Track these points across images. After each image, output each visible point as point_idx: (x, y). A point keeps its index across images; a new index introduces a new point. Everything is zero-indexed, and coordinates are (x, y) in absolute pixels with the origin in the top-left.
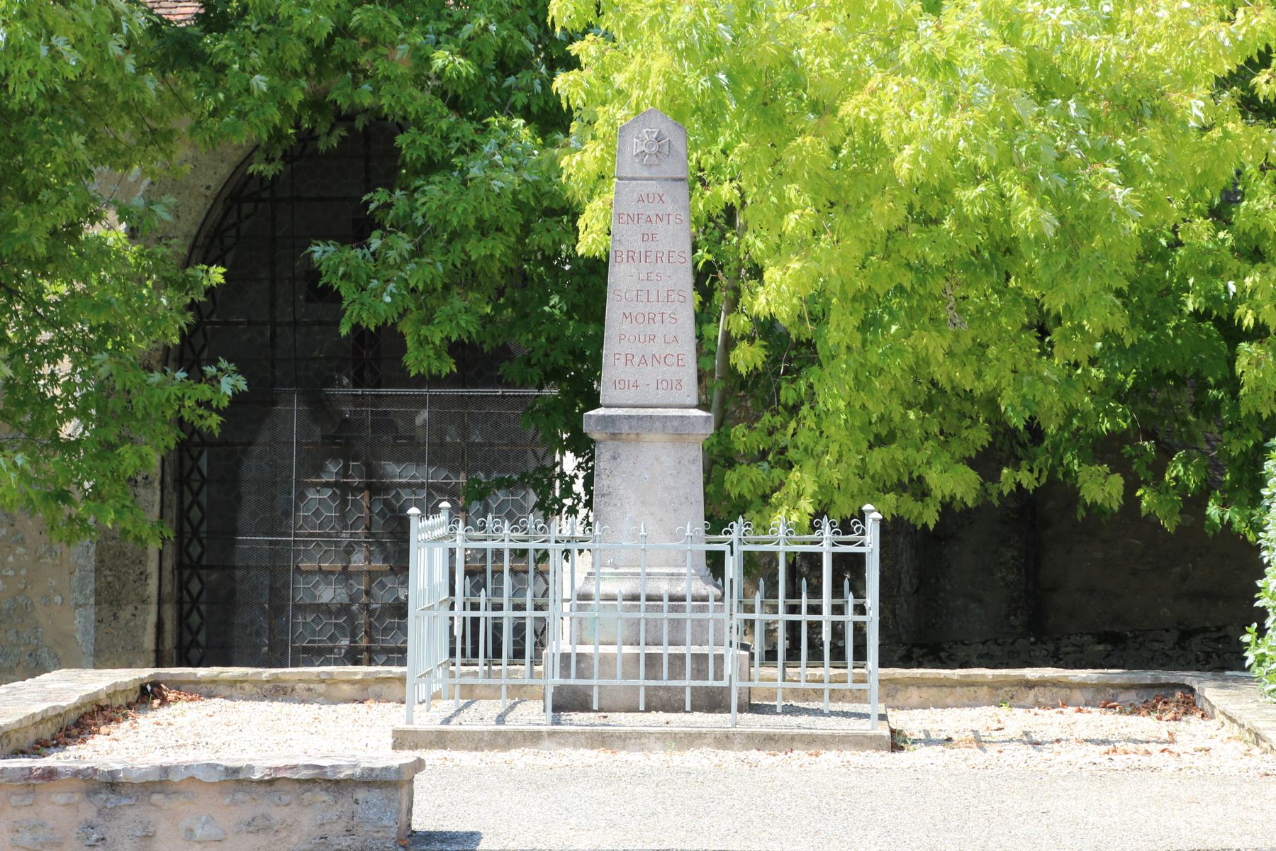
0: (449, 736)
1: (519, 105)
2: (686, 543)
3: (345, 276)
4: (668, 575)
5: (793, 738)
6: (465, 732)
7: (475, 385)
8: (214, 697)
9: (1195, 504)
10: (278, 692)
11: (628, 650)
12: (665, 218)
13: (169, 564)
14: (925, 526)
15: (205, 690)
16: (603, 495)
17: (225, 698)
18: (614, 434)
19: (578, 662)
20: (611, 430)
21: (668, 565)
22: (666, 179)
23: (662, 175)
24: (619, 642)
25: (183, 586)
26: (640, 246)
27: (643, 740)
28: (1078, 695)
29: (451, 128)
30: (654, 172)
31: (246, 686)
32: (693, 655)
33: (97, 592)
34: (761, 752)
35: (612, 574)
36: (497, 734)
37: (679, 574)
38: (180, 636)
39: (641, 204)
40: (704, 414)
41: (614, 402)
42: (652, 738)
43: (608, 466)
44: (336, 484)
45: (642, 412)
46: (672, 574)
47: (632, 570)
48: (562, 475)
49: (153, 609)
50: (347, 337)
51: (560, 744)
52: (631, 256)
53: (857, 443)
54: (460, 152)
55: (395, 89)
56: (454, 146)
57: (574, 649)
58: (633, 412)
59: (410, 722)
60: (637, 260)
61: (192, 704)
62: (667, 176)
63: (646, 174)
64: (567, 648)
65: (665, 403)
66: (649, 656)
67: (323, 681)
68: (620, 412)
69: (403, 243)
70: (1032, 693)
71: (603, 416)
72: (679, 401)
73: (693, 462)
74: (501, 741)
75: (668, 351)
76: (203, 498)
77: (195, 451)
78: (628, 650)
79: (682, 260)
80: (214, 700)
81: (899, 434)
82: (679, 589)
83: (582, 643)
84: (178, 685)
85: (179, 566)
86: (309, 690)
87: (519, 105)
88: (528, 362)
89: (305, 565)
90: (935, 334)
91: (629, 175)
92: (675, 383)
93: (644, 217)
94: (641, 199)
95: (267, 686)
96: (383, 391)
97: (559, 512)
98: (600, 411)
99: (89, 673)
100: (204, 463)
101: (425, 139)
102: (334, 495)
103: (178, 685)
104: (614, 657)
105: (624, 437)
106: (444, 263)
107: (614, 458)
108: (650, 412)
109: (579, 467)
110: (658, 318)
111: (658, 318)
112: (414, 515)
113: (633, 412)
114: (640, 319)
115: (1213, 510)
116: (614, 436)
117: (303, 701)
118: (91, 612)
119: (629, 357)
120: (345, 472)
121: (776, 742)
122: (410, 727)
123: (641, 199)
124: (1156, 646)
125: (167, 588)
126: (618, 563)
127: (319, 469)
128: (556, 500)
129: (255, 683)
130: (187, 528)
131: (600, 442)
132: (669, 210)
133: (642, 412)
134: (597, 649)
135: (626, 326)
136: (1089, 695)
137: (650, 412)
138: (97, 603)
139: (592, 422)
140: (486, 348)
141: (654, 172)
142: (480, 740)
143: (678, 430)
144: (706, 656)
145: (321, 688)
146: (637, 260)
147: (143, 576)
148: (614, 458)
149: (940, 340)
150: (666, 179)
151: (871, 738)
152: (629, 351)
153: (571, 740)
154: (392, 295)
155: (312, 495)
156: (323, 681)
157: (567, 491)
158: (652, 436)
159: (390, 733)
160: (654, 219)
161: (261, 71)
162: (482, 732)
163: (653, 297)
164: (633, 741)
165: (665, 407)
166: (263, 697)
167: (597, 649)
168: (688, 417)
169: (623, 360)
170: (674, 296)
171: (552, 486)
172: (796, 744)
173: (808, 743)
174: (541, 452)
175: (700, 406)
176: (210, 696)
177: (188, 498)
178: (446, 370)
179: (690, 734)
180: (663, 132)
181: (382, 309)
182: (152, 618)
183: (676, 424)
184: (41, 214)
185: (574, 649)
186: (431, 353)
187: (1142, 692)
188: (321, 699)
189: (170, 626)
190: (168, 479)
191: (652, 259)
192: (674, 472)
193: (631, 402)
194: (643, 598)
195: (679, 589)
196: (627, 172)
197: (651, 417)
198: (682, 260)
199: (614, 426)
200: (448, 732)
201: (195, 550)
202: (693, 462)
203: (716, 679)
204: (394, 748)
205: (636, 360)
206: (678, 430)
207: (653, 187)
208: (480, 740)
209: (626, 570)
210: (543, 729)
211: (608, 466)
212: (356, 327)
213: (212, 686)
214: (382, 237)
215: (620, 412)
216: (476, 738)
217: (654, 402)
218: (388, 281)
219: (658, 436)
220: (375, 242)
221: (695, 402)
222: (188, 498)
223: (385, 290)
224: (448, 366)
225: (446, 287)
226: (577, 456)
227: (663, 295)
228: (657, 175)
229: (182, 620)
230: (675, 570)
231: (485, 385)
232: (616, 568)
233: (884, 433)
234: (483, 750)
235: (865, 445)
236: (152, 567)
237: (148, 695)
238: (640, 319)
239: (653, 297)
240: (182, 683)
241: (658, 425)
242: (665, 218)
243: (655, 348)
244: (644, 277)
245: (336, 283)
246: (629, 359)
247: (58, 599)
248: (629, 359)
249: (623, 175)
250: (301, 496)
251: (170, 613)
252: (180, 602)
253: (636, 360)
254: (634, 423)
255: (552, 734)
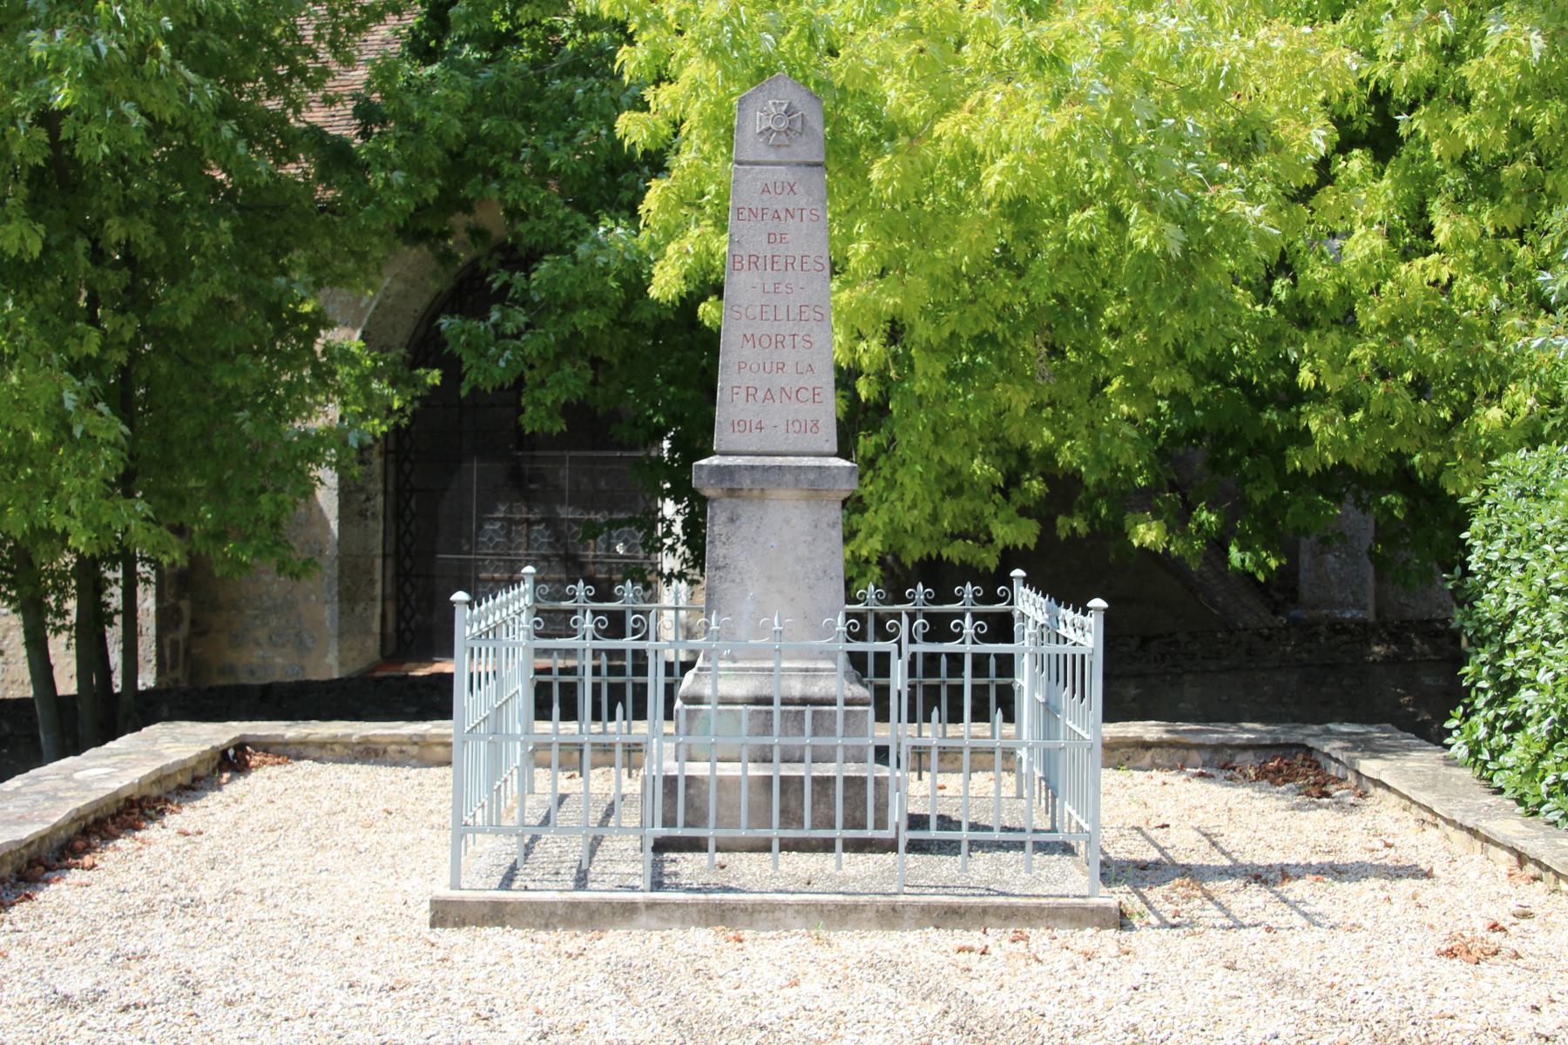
0: (508, 909)
1: (625, 201)
2: (836, 640)
3: (468, 345)
4: (801, 670)
5: (985, 911)
6: (531, 903)
7: (601, 449)
8: (303, 758)
9: (1218, 546)
10: (368, 753)
11: (756, 770)
12: (798, 214)
13: (389, 574)
14: (987, 569)
15: (294, 752)
16: (718, 568)
17: (314, 760)
18: (732, 490)
19: (687, 787)
20: (727, 485)
21: (801, 657)
22: (799, 164)
23: (794, 159)
24: (745, 757)
25: (399, 589)
26: (765, 250)
27: (779, 914)
28: (1195, 756)
29: (567, 218)
30: (783, 155)
31: (337, 748)
32: (847, 779)
33: (340, 593)
34: (942, 931)
35: (729, 669)
36: (575, 905)
37: (816, 670)
38: (398, 623)
39: (766, 196)
40: (848, 464)
41: (732, 448)
42: (790, 911)
43: (724, 531)
44: (504, 519)
45: (768, 461)
46: (807, 670)
47: (755, 665)
48: (663, 519)
49: (379, 604)
50: (466, 398)
51: (662, 919)
52: (754, 260)
53: (931, 493)
54: (573, 237)
55: (519, 185)
56: (568, 233)
57: (682, 768)
58: (757, 461)
59: (456, 885)
60: (761, 267)
61: (282, 769)
62: (800, 159)
63: (772, 157)
64: (671, 767)
65: (797, 449)
66: (785, 781)
67: (416, 743)
68: (740, 461)
69: (520, 317)
70: (1149, 754)
71: (718, 467)
72: (816, 447)
73: (834, 525)
74: (580, 915)
75: (801, 384)
76: (413, 528)
77: (407, 495)
78: (756, 770)
79: (819, 267)
80: (302, 763)
81: (966, 486)
82: (817, 689)
83: (690, 759)
84: (270, 748)
85: (397, 575)
86: (401, 752)
87: (625, 201)
88: (635, 424)
89: (483, 575)
90: (1019, 387)
91: (752, 159)
92: (810, 424)
93: (770, 213)
94: (766, 190)
95: (358, 748)
96: (537, 453)
97: (660, 549)
98: (715, 460)
99: (187, 727)
100: (413, 503)
101: (543, 226)
102: (502, 527)
103: (270, 748)
104: (736, 781)
105: (744, 493)
106: (555, 334)
107: (732, 520)
108: (778, 461)
109: (678, 512)
110: (789, 340)
111: (789, 340)
112: (461, 602)
113: (757, 461)
114: (766, 342)
115: (1235, 554)
116: (732, 492)
117: (395, 764)
118: (336, 607)
119: (751, 391)
120: (510, 510)
121: (962, 916)
122: (456, 895)
123: (766, 190)
124: (1124, 649)
125: (389, 590)
126: (736, 654)
127: (494, 509)
128: (660, 540)
129: (346, 744)
130: (402, 548)
131: (714, 500)
132: (803, 203)
133: (768, 461)
134: (713, 769)
135: (748, 351)
136: (1206, 756)
137: (778, 461)
138: (340, 600)
139: (704, 474)
140: (599, 412)
141: (783, 155)
142: (552, 914)
143: (813, 484)
144: (863, 780)
145: (414, 750)
146: (761, 267)
147: (372, 582)
148: (732, 520)
149: (1023, 395)
150: (799, 164)
151: (1092, 910)
152: (751, 384)
153: (678, 914)
154: (508, 361)
155: (488, 527)
156: (416, 743)
157: (668, 533)
158: (782, 493)
159: (427, 906)
160: (782, 215)
161: (401, 168)
162: (554, 904)
163: (782, 315)
164: (763, 915)
165: (797, 455)
166: (353, 760)
167: (713, 769)
168: (829, 468)
169: (744, 395)
170: (808, 313)
171: (655, 529)
172: (989, 920)
173: (1006, 918)
174: (648, 496)
175: (839, 455)
176: (299, 758)
177: (403, 527)
178: (557, 429)
179: (843, 906)
180: (795, 103)
181: (497, 373)
182: (378, 611)
183: (812, 476)
184: (190, 291)
185: (682, 768)
186: (544, 414)
187: (1260, 753)
188: (414, 762)
189: (391, 616)
190: (389, 515)
191: (780, 265)
192: (809, 538)
193: (753, 448)
194: (777, 701)
195: (816, 689)
196: (748, 155)
197: (780, 467)
198: (819, 267)
199: (732, 480)
200: (507, 904)
201: (408, 563)
202: (834, 525)
203: (876, 828)
204: (433, 925)
205: (761, 395)
206: (813, 484)
207: (783, 174)
208: (552, 914)
209: (748, 665)
210: (638, 897)
211: (724, 531)
212: (474, 390)
213: (301, 748)
214: (501, 310)
215: (740, 461)
216: (546, 911)
217: (783, 449)
218: (505, 350)
219: (789, 493)
220: (495, 316)
221: (835, 449)
222: (403, 527)
223: (501, 356)
224: (560, 426)
225: (558, 356)
226: (677, 503)
227: (794, 314)
228: (787, 159)
229: (399, 613)
230: (811, 665)
231: (608, 449)
232: (735, 661)
233: (953, 486)
234: (555, 929)
235: (938, 496)
236: (378, 575)
237: (233, 761)
238: (766, 342)
239: (782, 315)
240: (271, 744)
241: (789, 477)
242: (798, 214)
243: (786, 380)
244: (769, 288)
245: (458, 350)
246: (750, 393)
247: (313, 597)
248: (750, 393)
249: (743, 158)
250: (480, 527)
251: (391, 608)
252: (398, 600)
253: (761, 395)
254: (758, 475)
255: (651, 906)
